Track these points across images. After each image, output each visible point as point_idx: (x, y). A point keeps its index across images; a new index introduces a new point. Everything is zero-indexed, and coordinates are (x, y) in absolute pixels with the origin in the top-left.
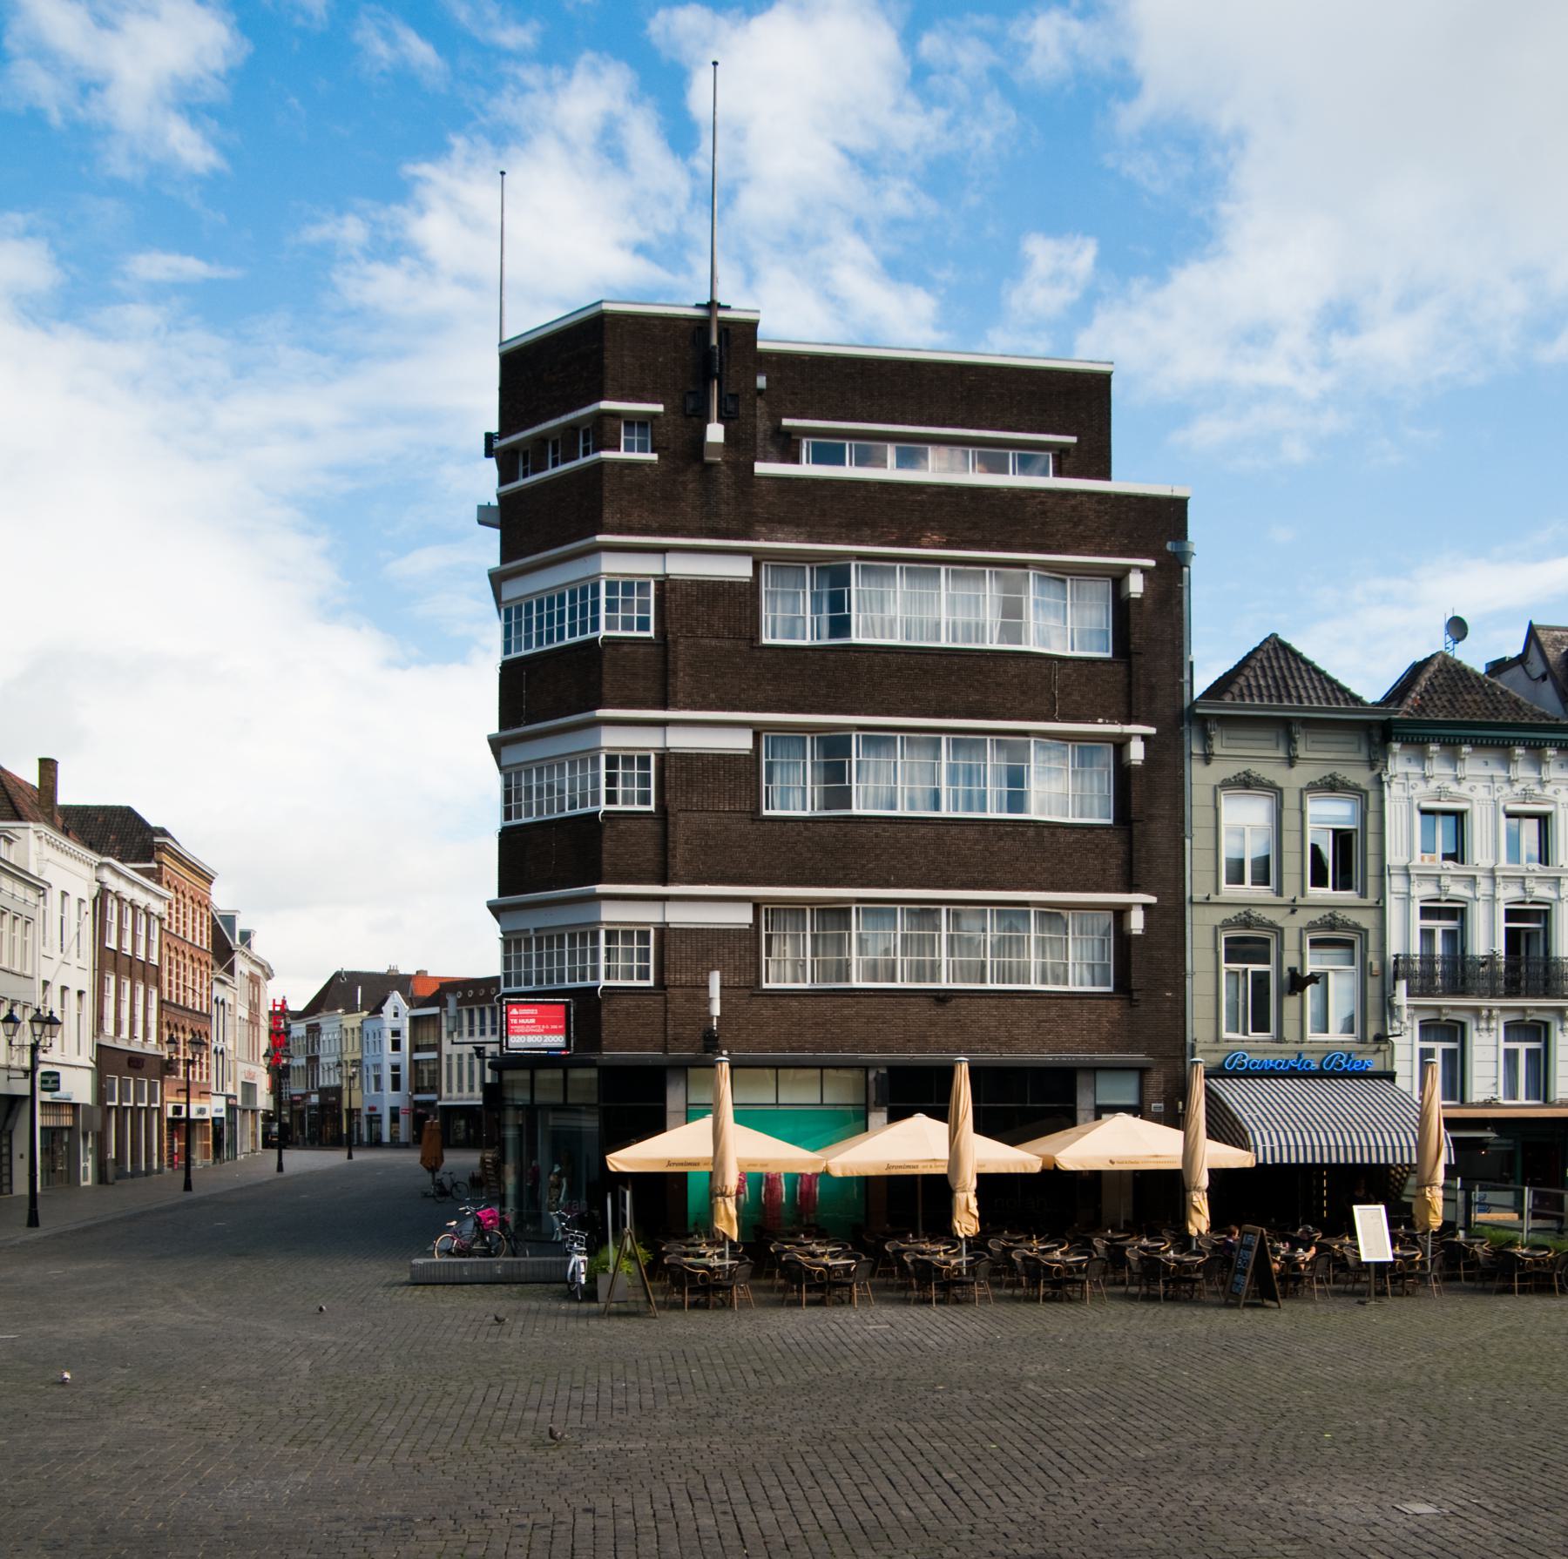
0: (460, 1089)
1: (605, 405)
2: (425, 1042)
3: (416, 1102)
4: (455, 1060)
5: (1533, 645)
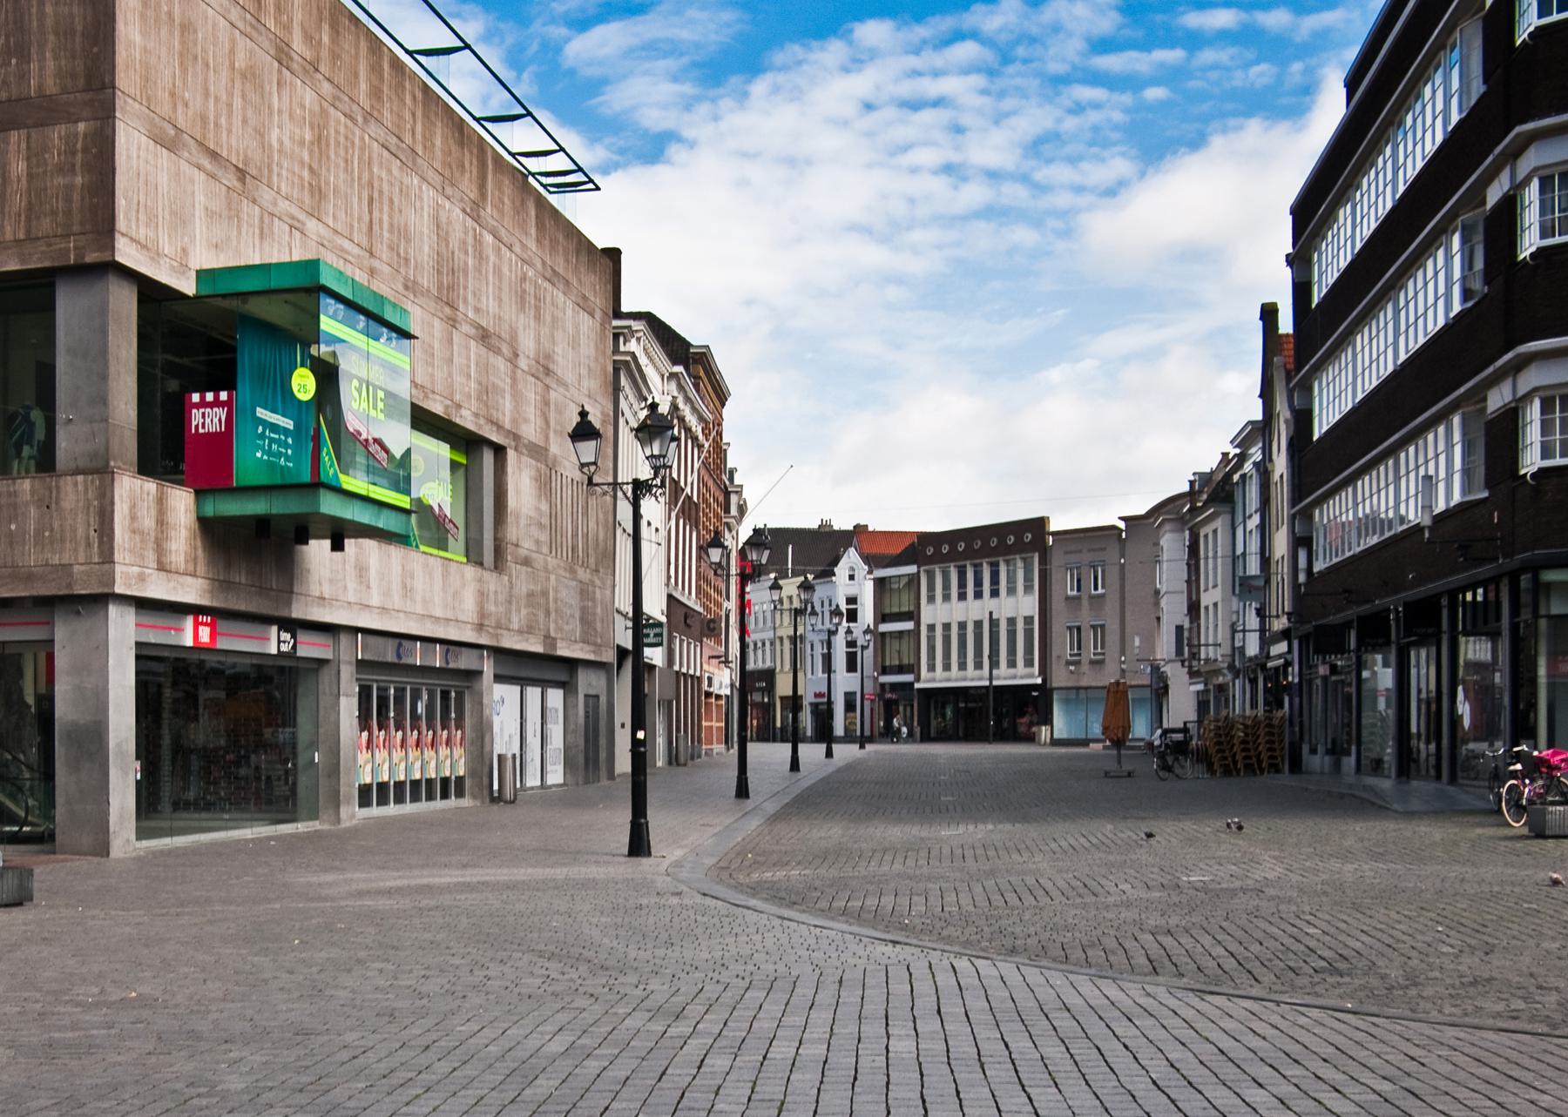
0: (947, 667)
1: (1518, 129)
2: (895, 610)
3: (883, 685)
4: (1020, 626)
5: (418, 57)
